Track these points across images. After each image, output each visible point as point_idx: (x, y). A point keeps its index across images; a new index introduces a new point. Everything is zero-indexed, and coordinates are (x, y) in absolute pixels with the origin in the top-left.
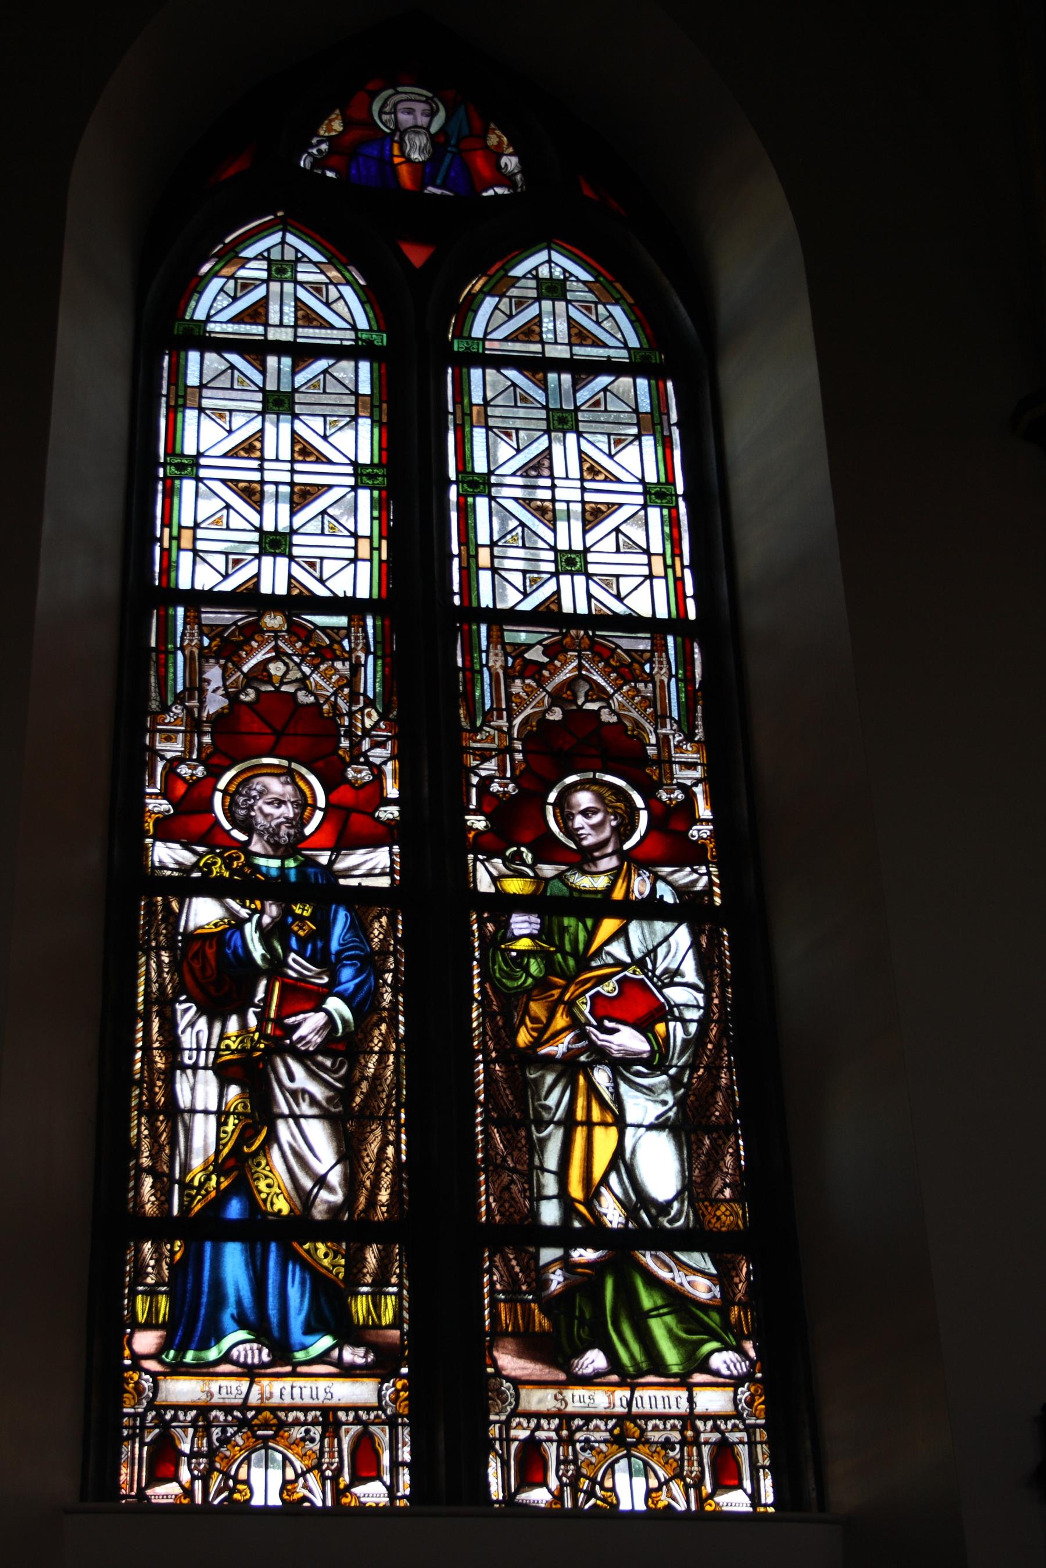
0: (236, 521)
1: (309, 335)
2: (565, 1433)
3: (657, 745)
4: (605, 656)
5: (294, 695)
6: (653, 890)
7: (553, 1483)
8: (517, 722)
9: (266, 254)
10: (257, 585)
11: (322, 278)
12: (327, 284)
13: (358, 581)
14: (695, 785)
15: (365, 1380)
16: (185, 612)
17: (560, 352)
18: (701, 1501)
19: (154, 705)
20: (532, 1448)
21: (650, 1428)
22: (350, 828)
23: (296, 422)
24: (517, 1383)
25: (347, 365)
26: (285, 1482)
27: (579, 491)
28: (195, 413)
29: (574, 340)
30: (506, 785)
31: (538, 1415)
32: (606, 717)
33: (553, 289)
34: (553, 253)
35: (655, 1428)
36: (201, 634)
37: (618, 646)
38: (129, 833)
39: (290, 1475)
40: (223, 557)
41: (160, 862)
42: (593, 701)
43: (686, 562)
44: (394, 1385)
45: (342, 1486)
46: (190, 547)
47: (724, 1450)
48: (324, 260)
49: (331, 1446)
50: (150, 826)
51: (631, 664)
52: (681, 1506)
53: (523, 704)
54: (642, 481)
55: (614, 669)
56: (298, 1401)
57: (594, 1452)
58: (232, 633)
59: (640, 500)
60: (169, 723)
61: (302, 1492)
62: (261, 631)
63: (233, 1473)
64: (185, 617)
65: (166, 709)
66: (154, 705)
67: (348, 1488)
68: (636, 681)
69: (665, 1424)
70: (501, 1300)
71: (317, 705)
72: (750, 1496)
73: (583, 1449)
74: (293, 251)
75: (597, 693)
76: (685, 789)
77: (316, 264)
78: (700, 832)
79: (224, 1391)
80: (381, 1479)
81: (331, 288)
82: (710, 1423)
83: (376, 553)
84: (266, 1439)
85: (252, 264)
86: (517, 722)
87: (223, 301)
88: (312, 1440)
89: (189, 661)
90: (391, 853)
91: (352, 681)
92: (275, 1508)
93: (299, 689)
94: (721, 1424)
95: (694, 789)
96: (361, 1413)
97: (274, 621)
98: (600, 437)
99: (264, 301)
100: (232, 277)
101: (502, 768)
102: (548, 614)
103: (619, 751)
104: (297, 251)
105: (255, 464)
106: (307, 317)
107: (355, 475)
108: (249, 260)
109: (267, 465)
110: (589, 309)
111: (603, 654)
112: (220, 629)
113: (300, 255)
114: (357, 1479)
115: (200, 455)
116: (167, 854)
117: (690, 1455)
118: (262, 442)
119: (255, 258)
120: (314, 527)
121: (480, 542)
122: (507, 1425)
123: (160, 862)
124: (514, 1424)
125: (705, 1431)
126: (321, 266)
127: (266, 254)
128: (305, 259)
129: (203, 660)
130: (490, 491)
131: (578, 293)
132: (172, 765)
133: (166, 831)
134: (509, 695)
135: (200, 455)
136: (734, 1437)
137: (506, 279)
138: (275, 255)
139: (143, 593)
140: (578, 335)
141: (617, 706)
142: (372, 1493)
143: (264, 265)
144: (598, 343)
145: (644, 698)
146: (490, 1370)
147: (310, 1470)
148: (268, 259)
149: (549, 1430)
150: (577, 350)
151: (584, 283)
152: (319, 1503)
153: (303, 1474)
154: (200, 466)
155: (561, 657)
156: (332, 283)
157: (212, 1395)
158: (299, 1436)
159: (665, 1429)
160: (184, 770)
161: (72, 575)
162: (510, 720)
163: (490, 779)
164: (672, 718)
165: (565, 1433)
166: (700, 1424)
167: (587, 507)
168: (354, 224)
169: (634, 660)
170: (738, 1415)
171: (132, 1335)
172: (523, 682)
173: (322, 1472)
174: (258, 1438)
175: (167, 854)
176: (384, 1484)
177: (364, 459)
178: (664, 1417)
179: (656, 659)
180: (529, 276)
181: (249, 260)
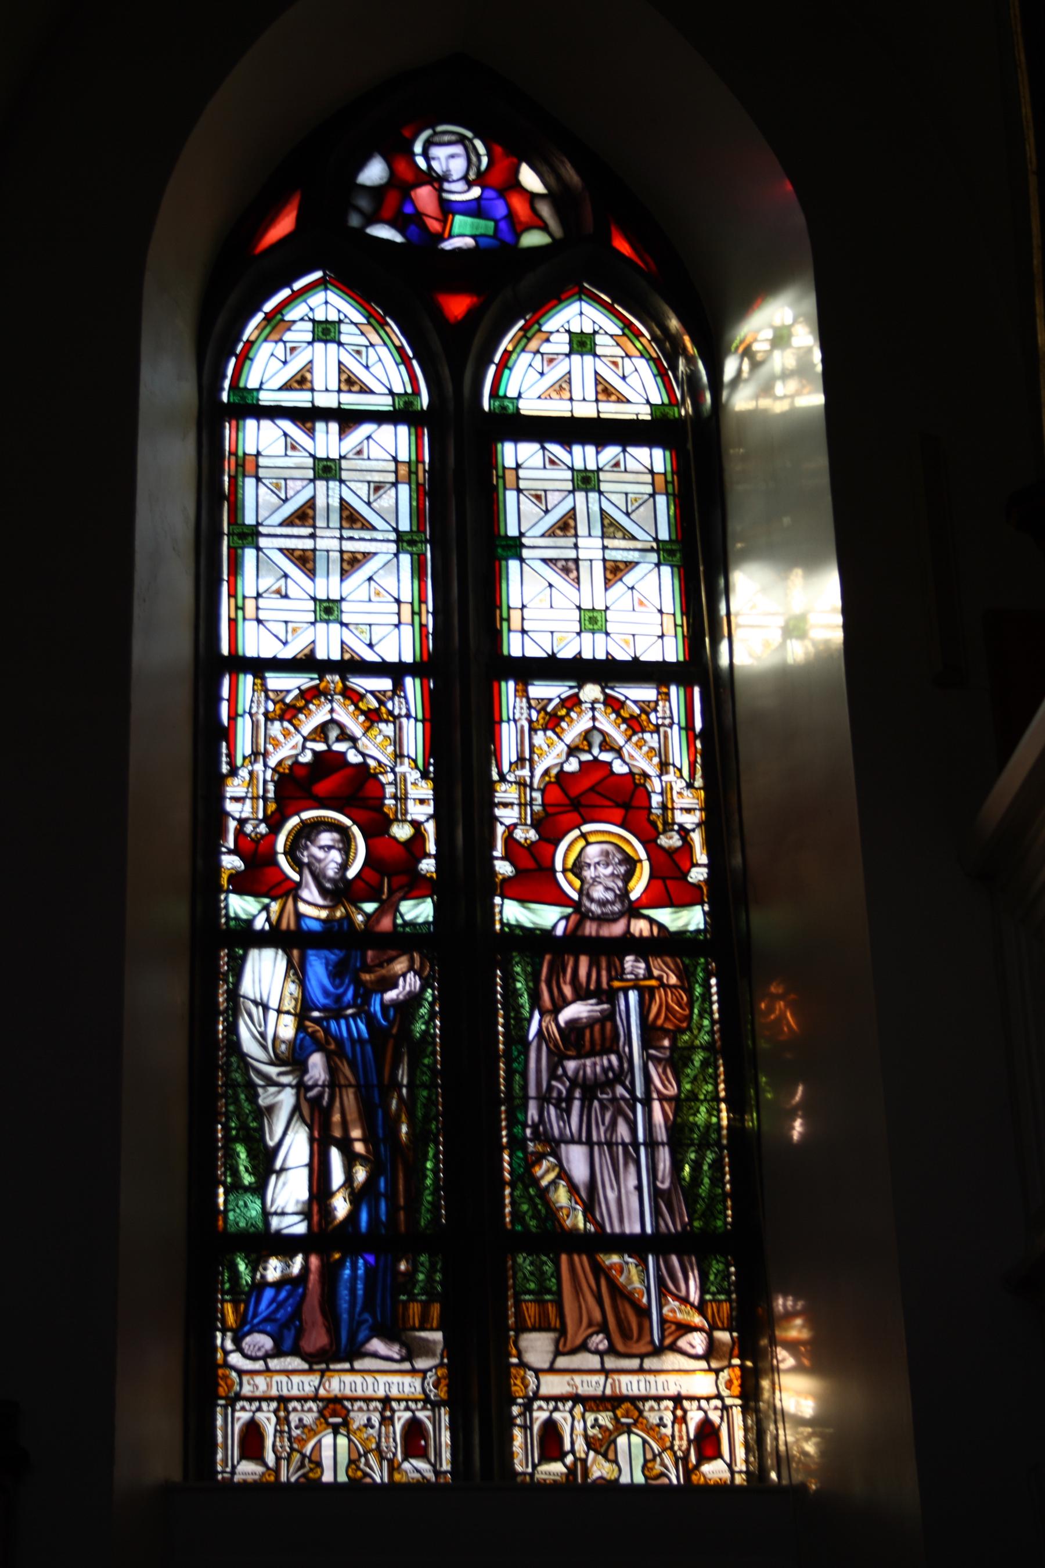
0: (293, 590)
1: (352, 401)
2: (282, 1414)
3: (662, 794)
4: (355, 701)
5: (610, 764)
7: (270, 1458)
8: (539, 771)
10: (313, 651)
11: (363, 341)
12: (367, 347)
13: (399, 645)
14: (427, 820)
16: (516, 684)
17: (326, 401)
18: (688, 1473)
19: (225, 769)
20: (551, 1428)
21: (356, 1407)
22: (670, 886)
23: (521, 495)
24: (241, 1373)
25: (387, 429)
26: (646, 1461)
27: (580, 545)
28: (515, 493)
29: (344, 387)
30: (528, 831)
31: (557, 1399)
32: (353, 758)
33: (582, 344)
35: (360, 1409)
36: (530, 707)
37: (627, 698)
38: (207, 887)
39: (649, 1456)
40: (284, 624)
41: (235, 913)
42: (607, 751)
43: (431, 609)
44: (436, 1373)
45: (690, 1466)
46: (254, 616)
47: (414, 1428)
49: (680, 1431)
50: (224, 881)
51: (639, 715)
52: (625, 1479)
53: (277, 745)
54: (396, 530)
55: (363, 712)
56: (653, 1392)
57: (306, 1430)
58: (296, 698)
59: (393, 547)
60: (505, 792)
61: (658, 1468)
62: (580, 702)
63: (308, 1453)
64: (516, 690)
65: (234, 772)
66: (225, 769)
67: (697, 1467)
68: (643, 731)
69: (302, 1406)
70: (548, 1301)
71: (364, 765)
72: (730, 1466)
73: (297, 1427)
75: (607, 745)
76: (416, 825)
77: (356, 324)
78: (428, 866)
79: (585, 1384)
80: (721, 1457)
82: (403, 1404)
83: (416, 618)
84: (628, 1425)
86: (539, 771)
87: (276, 364)
88: (373, 1427)
89: (255, 726)
91: (397, 741)
92: (343, 1484)
93: (351, 748)
94: (412, 1405)
95: (426, 825)
96: (410, 1403)
97: (591, 692)
98: (359, 485)
99: (309, 366)
100: (537, 352)
101: (255, 810)
102: (306, 663)
103: (621, 798)
105: (308, 531)
106: (350, 382)
107: (397, 542)
109: (319, 532)
110: (615, 364)
111: (352, 696)
112: (284, 694)
114: (702, 1459)
115: (258, 524)
116: (241, 906)
117: (680, 1431)
118: (575, 520)
120: (363, 593)
121: (247, 594)
122: (528, 1407)
123: (235, 913)
124: (238, 1407)
125: (399, 1410)
126: (362, 327)
129: (269, 723)
130: (257, 542)
132: (511, 829)
133: (242, 884)
134: (532, 746)
135: (258, 524)
136: (421, 1415)
137: (282, 324)
139: (216, 664)
140: (605, 391)
141: (636, 758)
142: (714, 1470)
144: (365, 390)
145: (652, 749)
146: (514, 1360)
147: (664, 1450)
149: (565, 1411)
150: (602, 406)
151: (356, 324)
152: (378, 1480)
153: (660, 1454)
154: (260, 534)
155: (577, 709)
156: (627, 356)
157: (577, 1388)
158: (362, 1423)
159: (368, 1410)
160: (519, 834)
161: (159, 645)
162: (532, 770)
163: (515, 826)
164: (674, 766)
165: (282, 1414)
166: (394, 1404)
167: (345, 556)
168: (404, 287)
169: (643, 710)
170: (719, 1396)
171: (517, 1337)
172: (282, 725)
173: (675, 1453)
174: (328, 1424)
175: (241, 906)
176: (725, 1462)
177: (405, 526)
178: (367, 1400)
179: (659, 708)
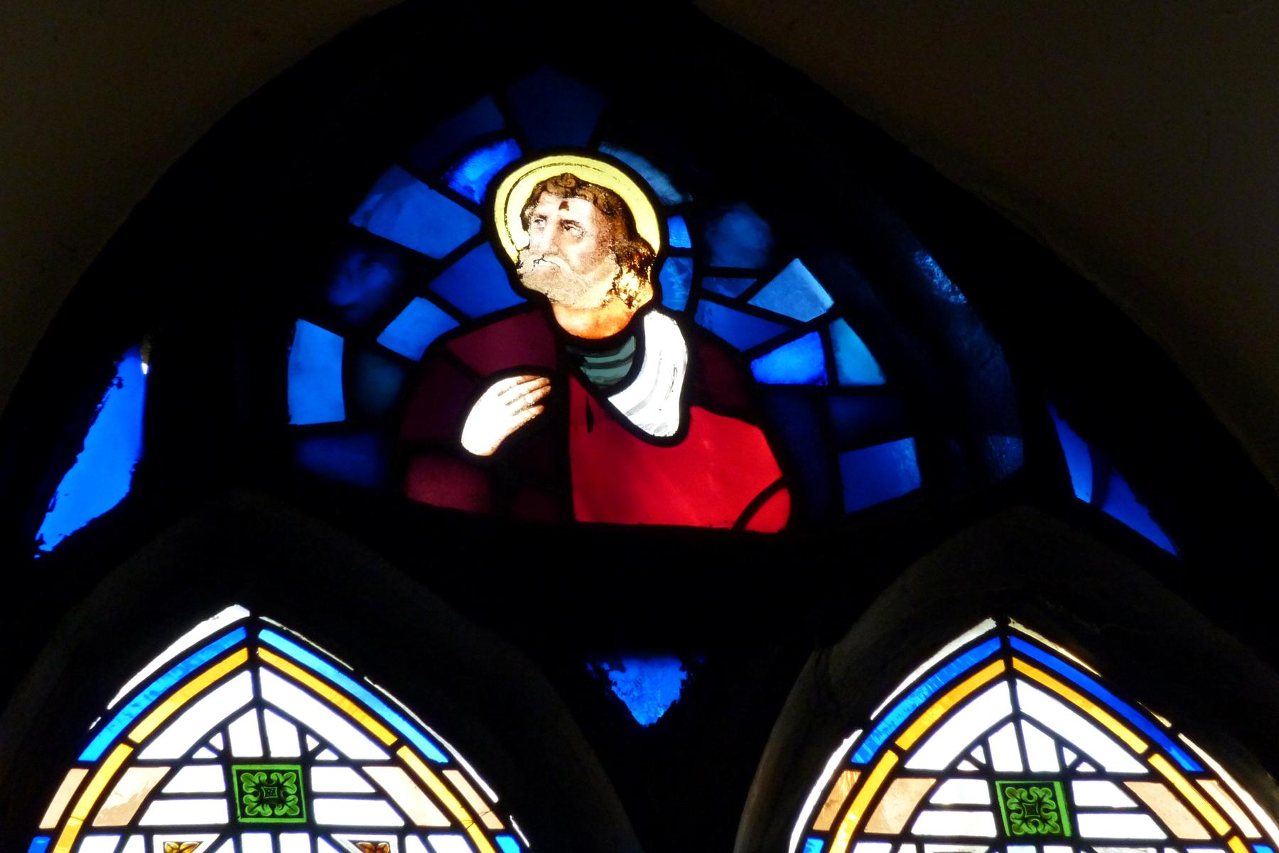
9: (217, 741)
77: (358, 766)
85: (187, 779)
113: (312, 744)
119: (952, 772)
143: (978, 791)
148: (985, 772)
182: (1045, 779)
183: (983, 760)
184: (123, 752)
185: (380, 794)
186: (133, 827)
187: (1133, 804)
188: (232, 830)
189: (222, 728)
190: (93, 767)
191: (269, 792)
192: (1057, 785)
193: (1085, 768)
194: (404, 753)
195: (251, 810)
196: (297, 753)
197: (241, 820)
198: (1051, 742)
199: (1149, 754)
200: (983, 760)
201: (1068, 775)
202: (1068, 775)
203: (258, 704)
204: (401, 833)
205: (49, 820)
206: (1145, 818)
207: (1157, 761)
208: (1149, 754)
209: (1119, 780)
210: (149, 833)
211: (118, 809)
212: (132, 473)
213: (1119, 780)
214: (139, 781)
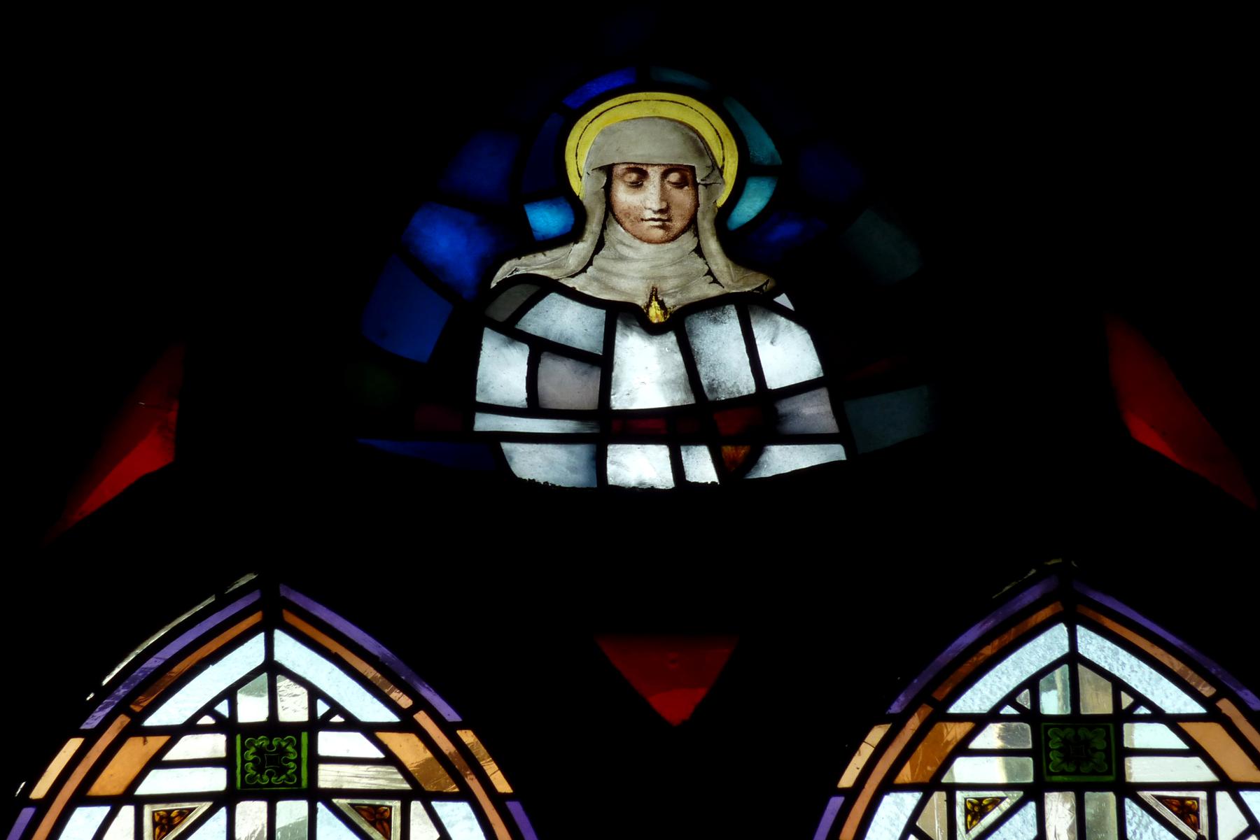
6: (649, 305)
9: (223, 708)
11: (1196, 770)
12: (1210, 788)
15: (602, 329)
34: (1081, 631)
48: (1196, 708)
74: (303, 693)
81: (1223, 799)
85: (187, 747)
90: (766, 283)
104: (1119, 686)
108: (174, 733)
119: (191, 727)
127: (223, 708)
128: (1143, 710)
131: (345, 760)
138: (1052, 703)
143: (215, 745)
148: (227, 726)
180: (1008, 710)
181: (174, 733)
182: (295, 728)
183: (1028, 705)
184: (122, 721)
185: (390, 759)
186: (127, 796)
187: (378, 754)
188: (226, 800)
189: (230, 694)
190: (91, 738)
191: (271, 762)
192: (304, 736)
193: (337, 719)
194: (422, 718)
195: (290, 779)
196: (303, 716)
197: (1048, 779)
198: (1108, 685)
199: (1216, 697)
200: (1028, 705)
201: (316, 725)
202: (1123, 716)
203: (272, 668)
204: (405, 798)
205: (848, 779)
206: (1197, 761)
207: (1225, 706)
208: (1216, 697)
209: (370, 731)
210: (951, 789)
211: (111, 781)
212: (546, 483)
213: (370, 731)
214: (134, 752)
